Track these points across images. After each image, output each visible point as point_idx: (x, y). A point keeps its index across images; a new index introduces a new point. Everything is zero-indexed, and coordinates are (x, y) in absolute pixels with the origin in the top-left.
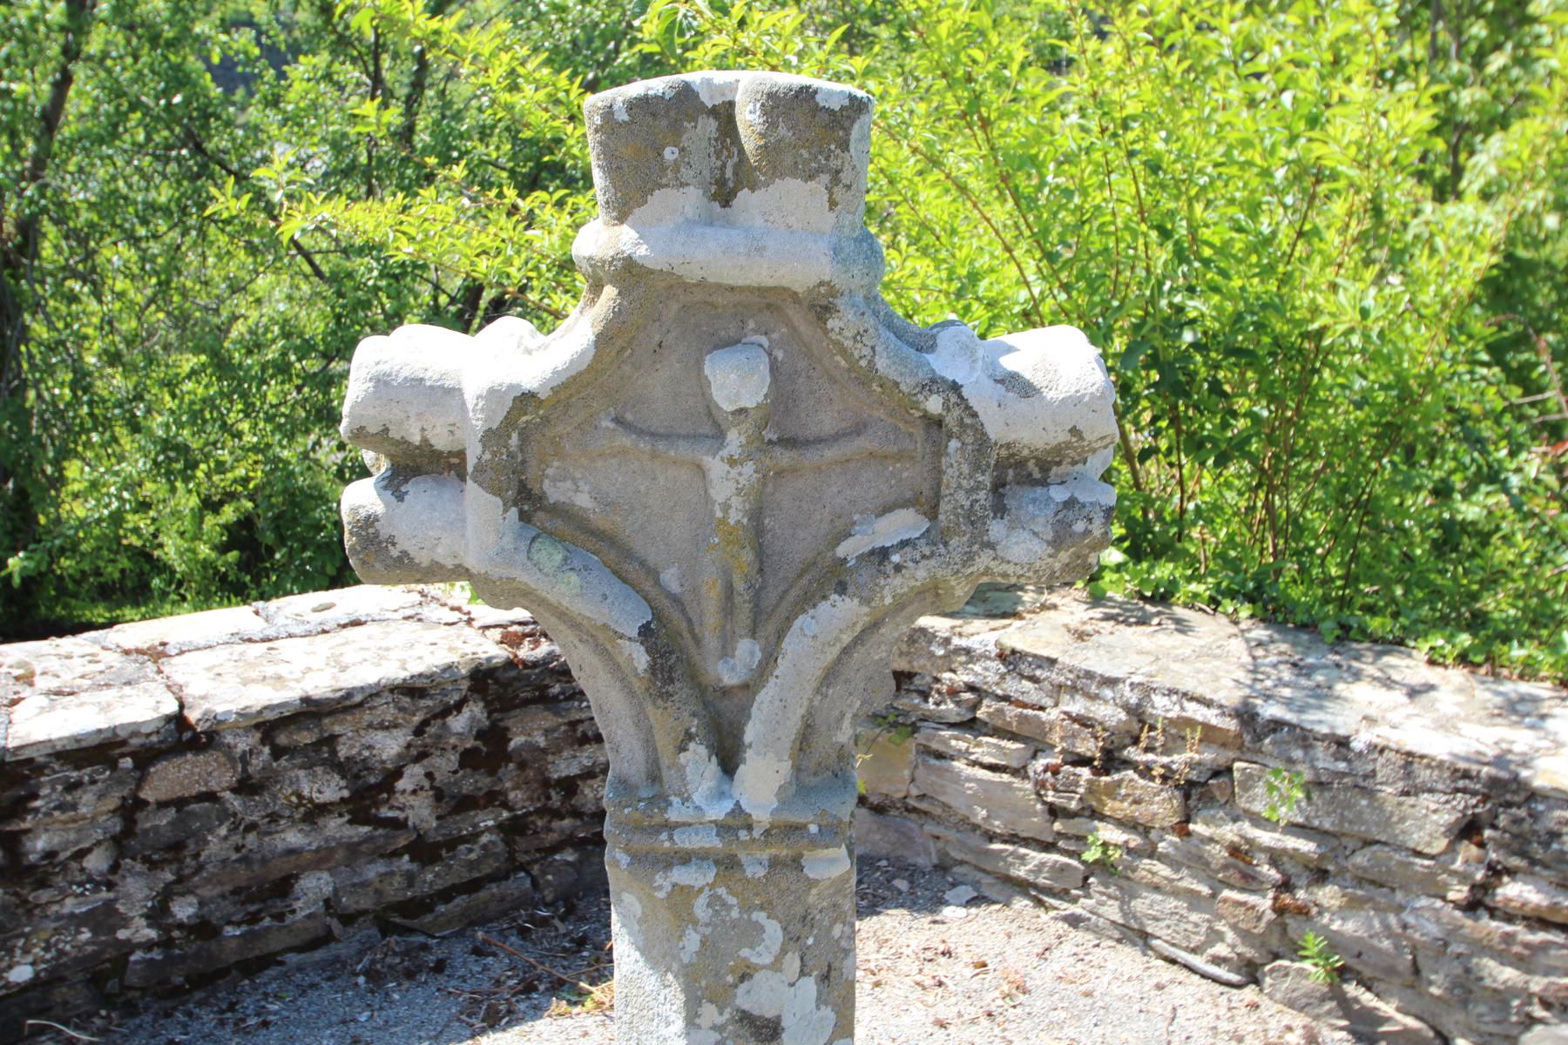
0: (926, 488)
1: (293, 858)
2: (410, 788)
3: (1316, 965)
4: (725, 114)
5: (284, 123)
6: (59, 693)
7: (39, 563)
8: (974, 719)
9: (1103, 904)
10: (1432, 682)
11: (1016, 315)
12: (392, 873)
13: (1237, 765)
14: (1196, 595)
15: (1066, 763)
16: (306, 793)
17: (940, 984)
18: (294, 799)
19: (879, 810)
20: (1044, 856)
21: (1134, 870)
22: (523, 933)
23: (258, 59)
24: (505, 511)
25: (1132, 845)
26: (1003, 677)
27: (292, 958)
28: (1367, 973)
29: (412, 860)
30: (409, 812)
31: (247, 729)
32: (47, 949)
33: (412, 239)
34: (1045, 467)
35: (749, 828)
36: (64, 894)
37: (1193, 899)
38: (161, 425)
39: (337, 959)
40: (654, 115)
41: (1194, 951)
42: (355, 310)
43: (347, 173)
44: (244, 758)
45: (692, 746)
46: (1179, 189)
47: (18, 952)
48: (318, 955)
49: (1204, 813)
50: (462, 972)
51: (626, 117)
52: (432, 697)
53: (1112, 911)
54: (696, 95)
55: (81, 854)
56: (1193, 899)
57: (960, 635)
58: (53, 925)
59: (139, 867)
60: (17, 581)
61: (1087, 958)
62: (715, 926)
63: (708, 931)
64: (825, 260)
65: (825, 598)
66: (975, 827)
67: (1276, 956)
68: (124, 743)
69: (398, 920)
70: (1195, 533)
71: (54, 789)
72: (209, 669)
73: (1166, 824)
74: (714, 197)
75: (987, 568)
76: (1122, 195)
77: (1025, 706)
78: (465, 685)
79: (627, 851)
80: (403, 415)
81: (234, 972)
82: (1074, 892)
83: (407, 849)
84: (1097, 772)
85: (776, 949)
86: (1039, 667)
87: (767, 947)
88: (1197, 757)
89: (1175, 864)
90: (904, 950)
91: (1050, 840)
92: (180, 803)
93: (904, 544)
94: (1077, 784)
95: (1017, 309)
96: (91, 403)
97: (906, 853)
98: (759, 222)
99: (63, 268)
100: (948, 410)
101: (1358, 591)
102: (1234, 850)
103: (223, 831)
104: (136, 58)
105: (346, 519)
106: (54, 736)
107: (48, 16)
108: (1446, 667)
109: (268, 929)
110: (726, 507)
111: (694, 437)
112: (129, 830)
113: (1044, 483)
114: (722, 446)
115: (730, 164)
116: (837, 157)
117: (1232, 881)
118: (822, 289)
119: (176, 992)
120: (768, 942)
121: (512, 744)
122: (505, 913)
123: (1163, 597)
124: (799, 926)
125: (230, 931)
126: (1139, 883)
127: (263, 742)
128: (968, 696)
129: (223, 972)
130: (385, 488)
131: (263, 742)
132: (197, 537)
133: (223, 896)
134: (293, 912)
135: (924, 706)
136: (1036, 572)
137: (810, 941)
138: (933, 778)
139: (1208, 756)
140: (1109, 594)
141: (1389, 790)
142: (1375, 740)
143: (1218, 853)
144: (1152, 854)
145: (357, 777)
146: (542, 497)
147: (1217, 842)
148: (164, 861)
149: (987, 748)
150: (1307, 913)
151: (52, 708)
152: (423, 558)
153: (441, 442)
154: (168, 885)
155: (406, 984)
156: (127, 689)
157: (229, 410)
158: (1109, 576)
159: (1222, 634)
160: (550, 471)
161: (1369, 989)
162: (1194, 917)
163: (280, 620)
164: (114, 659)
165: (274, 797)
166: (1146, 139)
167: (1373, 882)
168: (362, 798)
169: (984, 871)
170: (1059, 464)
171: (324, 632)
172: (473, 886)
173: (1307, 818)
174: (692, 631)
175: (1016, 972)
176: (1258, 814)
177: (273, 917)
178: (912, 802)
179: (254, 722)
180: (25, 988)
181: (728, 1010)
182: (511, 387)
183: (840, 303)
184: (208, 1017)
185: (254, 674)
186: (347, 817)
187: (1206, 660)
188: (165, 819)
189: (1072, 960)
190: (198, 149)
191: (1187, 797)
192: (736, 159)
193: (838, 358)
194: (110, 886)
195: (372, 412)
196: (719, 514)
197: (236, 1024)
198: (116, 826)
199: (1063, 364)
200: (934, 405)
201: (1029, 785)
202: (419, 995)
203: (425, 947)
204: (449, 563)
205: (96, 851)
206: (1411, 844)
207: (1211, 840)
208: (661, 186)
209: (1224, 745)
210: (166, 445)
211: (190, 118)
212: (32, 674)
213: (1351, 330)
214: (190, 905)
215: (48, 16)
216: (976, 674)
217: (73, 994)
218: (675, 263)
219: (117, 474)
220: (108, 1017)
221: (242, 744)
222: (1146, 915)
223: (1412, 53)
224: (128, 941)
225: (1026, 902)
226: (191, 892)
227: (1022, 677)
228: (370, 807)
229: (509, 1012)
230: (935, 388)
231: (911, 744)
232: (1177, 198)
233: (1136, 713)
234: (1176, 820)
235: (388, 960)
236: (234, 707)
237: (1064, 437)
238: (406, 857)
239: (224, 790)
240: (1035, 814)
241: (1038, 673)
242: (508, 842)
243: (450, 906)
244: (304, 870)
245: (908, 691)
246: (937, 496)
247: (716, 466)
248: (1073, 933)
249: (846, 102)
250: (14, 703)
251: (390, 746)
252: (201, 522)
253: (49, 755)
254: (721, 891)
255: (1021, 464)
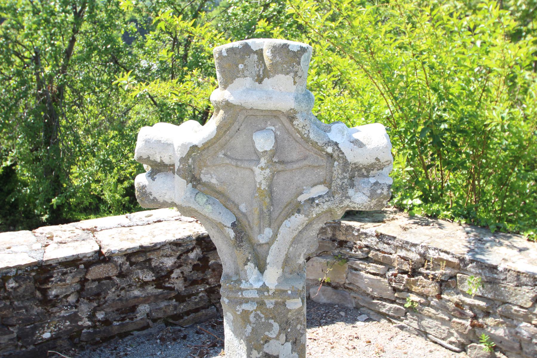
0: (328, 179)
1: (136, 299)
2: (176, 277)
3: (486, 345)
4: (260, 53)
5: (144, 54)
6: (61, 243)
7: (62, 201)
8: (368, 257)
9: (412, 322)
10: (528, 247)
11: (384, 119)
12: (169, 305)
13: (458, 275)
14: (446, 216)
15: (399, 273)
16: (141, 278)
17: (354, 348)
18: (137, 279)
19: (335, 288)
20: (392, 305)
21: (422, 311)
22: (213, 327)
23: (136, 32)
24: (187, 184)
25: (422, 302)
26: (377, 243)
27: (136, 333)
28: (504, 349)
29: (176, 301)
30: (175, 285)
31: (122, 256)
32: (55, 328)
33: (176, 95)
34: (368, 172)
35: (268, 291)
36: (61, 309)
37: (443, 321)
38: (102, 155)
39: (151, 334)
40: (235, 54)
41: (443, 339)
42: (166, 116)
43: (165, 70)
44: (121, 266)
45: (249, 263)
46: (440, 75)
47: (46, 328)
48: (145, 332)
49: (447, 291)
50: (192, 339)
51: (226, 55)
52: (183, 246)
53: (415, 325)
54: (250, 47)
55: (67, 296)
56: (443, 321)
57: (363, 228)
58: (58, 320)
59: (85, 301)
60: (55, 207)
61: (406, 341)
62: (257, 324)
63: (254, 325)
64: (292, 101)
65: (293, 214)
66: (368, 294)
67: (472, 342)
68: (81, 260)
69: (171, 321)
70: (448, 194)
71: (58, 275)
72: (110, 236)
73: (433, 295)
74: (256, 81)
75: (348, 205)
76: (420, 76)
77: (385, 253)
78: (194, 243)
79: (227, 298)
80: (154, 153)
81: (117, 337)
82: (402, 318)
83: (175, 297)
84: (410, 276)
85: (277, 332)
86: (390, 239)
87: (274, 332)
88: (444, 272)
89: (437, 309)
90: (343, 336)
91: (394, 299)
92: (99, 280)
93: (320, 196)
94: (403, 281)
95: (384, 116)
96: (79, 147)
97: (344, 303)
98: (271, 89)
99: (72, 102)
100: (334, 152)
101: (506, 215)
102: (457, 304)
103: (113, 290)
104: (96, 33)
105: (136, 186)
106: (58, 257)
107: (67, 19)
108: (534, 242)
109: (128, 323)
110: (260, 184)
111: (250, 161)
112: (82, 289)
113: (368, 177)
114: (259, 163)
115: (261, 69)
116: (296, 67)
117: (456, 315)
118: (291, 111)
119: (97, 343)
120: (274, 330)
121: (210, 263)
122: (207, 320)
123: (435, 216)
124: (285, 325)
125: (115, 323)
126: (424, 315)
127: (127, 260)
128: (366, 249)
129: (113, 337)
130: (149, 176)
131: (127, 260)
132: (115, 192)
133: (113, 312)
134: (136, 317)
135: (351, 252)
136: (365, 207)
137: (289, 330)
138: (354, 277)
139: (448, 271)
140: (416, 215)
141: (511, 284)
142: (506, 267)
143: (451, 305)
144: (429, 305)
145: (158, 273)
146: (200, 180)
147: (451, 301)
148: (94, 299)
149: (372, 267)
150: (483, 327)
151: (58, 248)
152: (161, 200)
153: (167, 161)
154: (95, 307)
155: (173, 343)
156: (83, 242)
157: (125, 150)
158: (416, 209)
159: (455, 229)
160: (203, 171)
161: (504, 354)
162: (443, 327)
163: (134, 220)
164: (80, 232)
165: (130, 279)
166: (429, 58)
167: (506, 317)
168: (160, 280)
169: (371, 310)
170: (373, 170)
171: (149, 224)
172: (197, 310)
173: (483, 294)
174: (249, 225)
175: (381, 345)
176: (465, 292)
177: (129, 319)
178: (346, 285)
179: (124, 253)
180: (48, 340)
181: (261, 352)
182: (189, 143)
183: (298, 116)
184: (107, 352)
185: (125, 238)
186: (155, 286)
187: (451, 239)
188: (94, 285)
189: (401, 341)
190: (116, 62)
191: (441, 285)
192: (263, 68)
193: (297, 134)
194: (76, 307)
195: (144, 151)
196: (258, 186)
197: (116, 354)
198: (78, 287)
199: (373, 138)
200: (330, 150)
201: (386, 280)
202: (177, 347)
203: (180, 331)
204: (170, 201)
205: (71, 296)
206: (519, 304)
207: (449, 301)
208: (238, 77)
209: (454, 268)
210: (104, 161)
211: (113, 52)
212: (53, 237)
213: (498, 124)
214: (102, 314)
215: (67, 19)
216: (368, 242)
217: (63, 343)
218: (242, 102)
219: (88, 171)
220: (75, 351)
221: (120, 261)
222: (426, 326)
223: (533, 27)
224: (82, 325)
225: (385, 321)
226: (103, 310)
227: (384, 243)
228: (162, 283)
229: (207, 353)
230: (329, 144)
231: (346, 265)
232: (440, 78)
233: (423, 256)
234: (437, 293)
235: (168, 334)
236: (118, 248)
237: (373, 161)
238: (174, 300)
239: (114, 276)
240: (388, 290)
241: (390, 242)
242: (208, 296)
243: (189, 317)
244: (140, 303)
245: (345, 247)
246: (331, 181)
247: (257, 170)
248: (401, 332)
249: (299, 49)
250: (46, 246)
251: (169, 262)
252: (117, 187)
253: (57, 263)
254: (259, 312)
255: (360, 170)
